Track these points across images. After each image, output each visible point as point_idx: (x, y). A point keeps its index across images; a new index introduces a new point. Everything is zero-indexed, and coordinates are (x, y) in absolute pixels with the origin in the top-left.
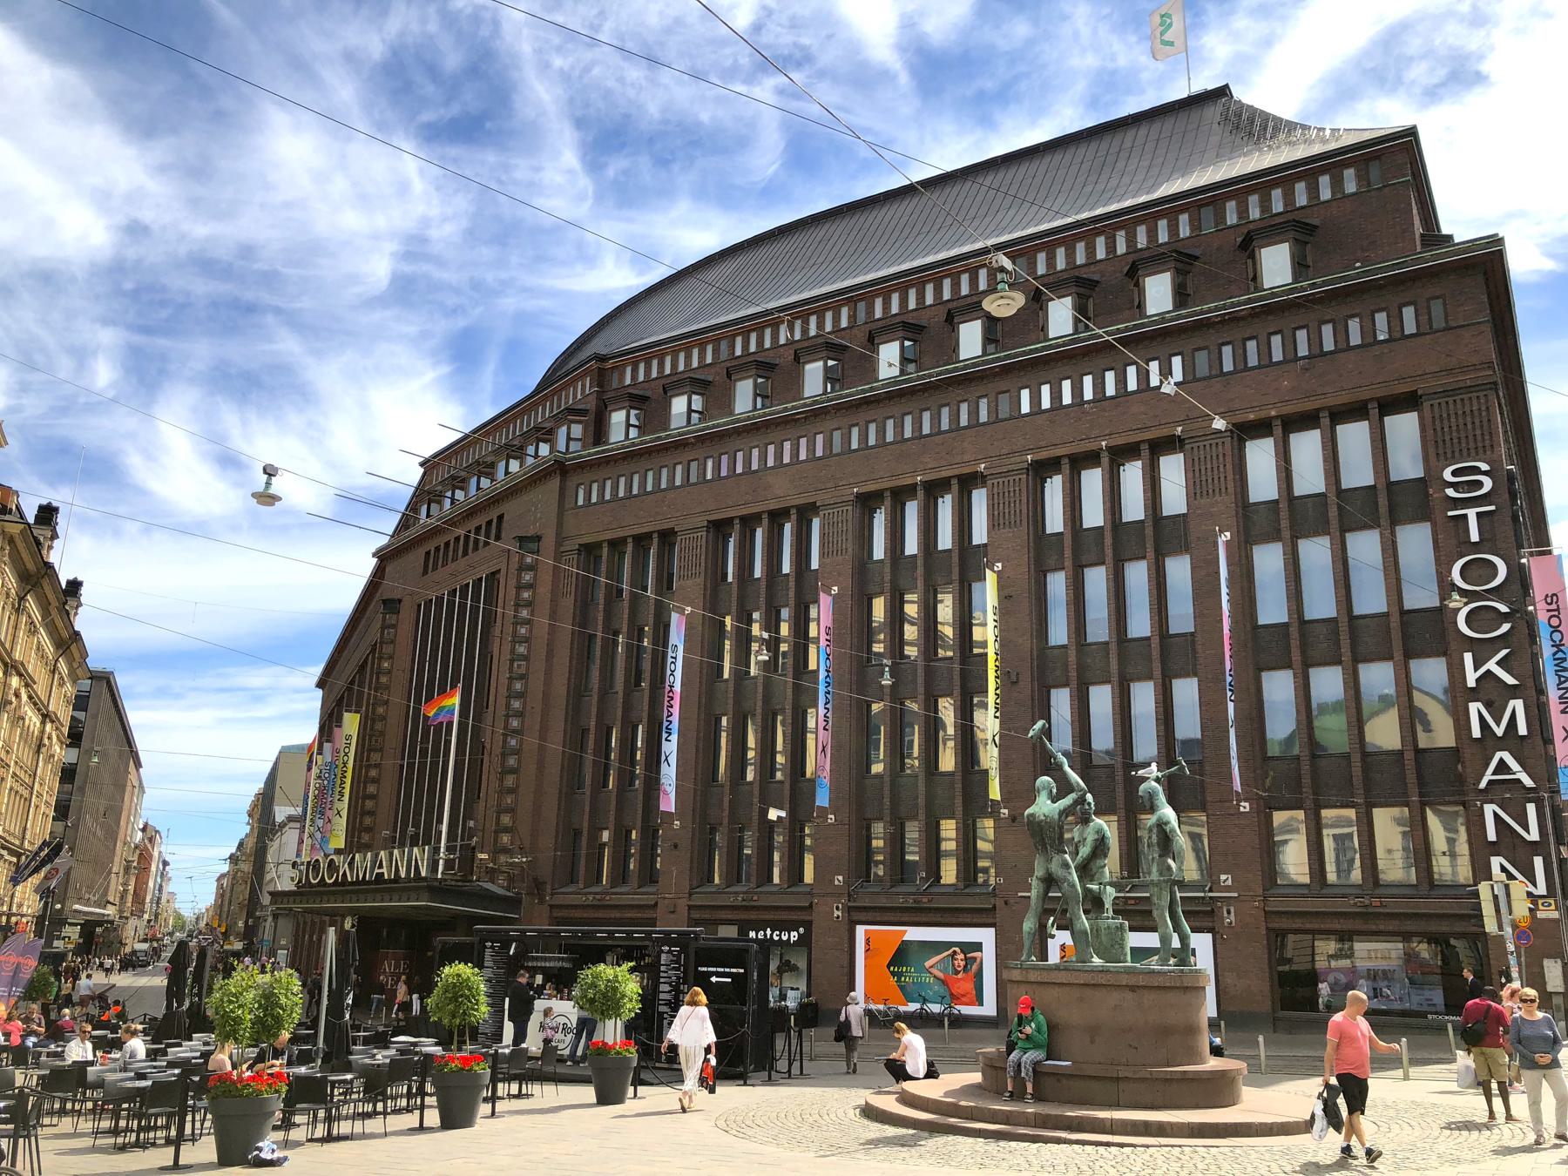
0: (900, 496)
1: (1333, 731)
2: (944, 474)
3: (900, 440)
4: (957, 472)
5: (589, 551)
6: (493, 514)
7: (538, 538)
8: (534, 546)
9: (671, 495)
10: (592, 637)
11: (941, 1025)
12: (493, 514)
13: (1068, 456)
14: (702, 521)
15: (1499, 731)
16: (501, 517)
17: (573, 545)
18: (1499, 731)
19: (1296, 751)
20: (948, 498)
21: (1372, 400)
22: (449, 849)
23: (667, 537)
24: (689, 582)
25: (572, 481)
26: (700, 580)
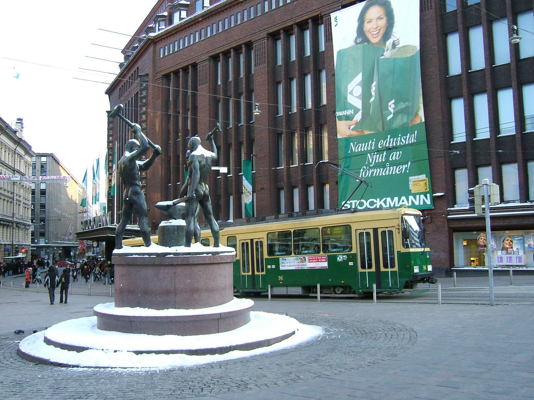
0: (288, 31)
1: (486, 174)
2: (305, 18)
3: (263, 13)
4: (310, 16)
5: (167, 76)
6: (135, 68)
7: (147, 75)
8: (146, 79)
9: (179, 53)
10: (170, 115)
11: (509, 274)
12: (135, 68)
13: (311, 18)
14: (264, 34)
15: (392, 206)
16: (138, 68)
17: (159, 76)
18: (392, 206)
19: (238, 258)
20: (323, 26)
21: (242, 44)
22: (118, 209)
23: (194, 66)
24: (203, 86)
25: (158, 46)
26: (207, 85)
